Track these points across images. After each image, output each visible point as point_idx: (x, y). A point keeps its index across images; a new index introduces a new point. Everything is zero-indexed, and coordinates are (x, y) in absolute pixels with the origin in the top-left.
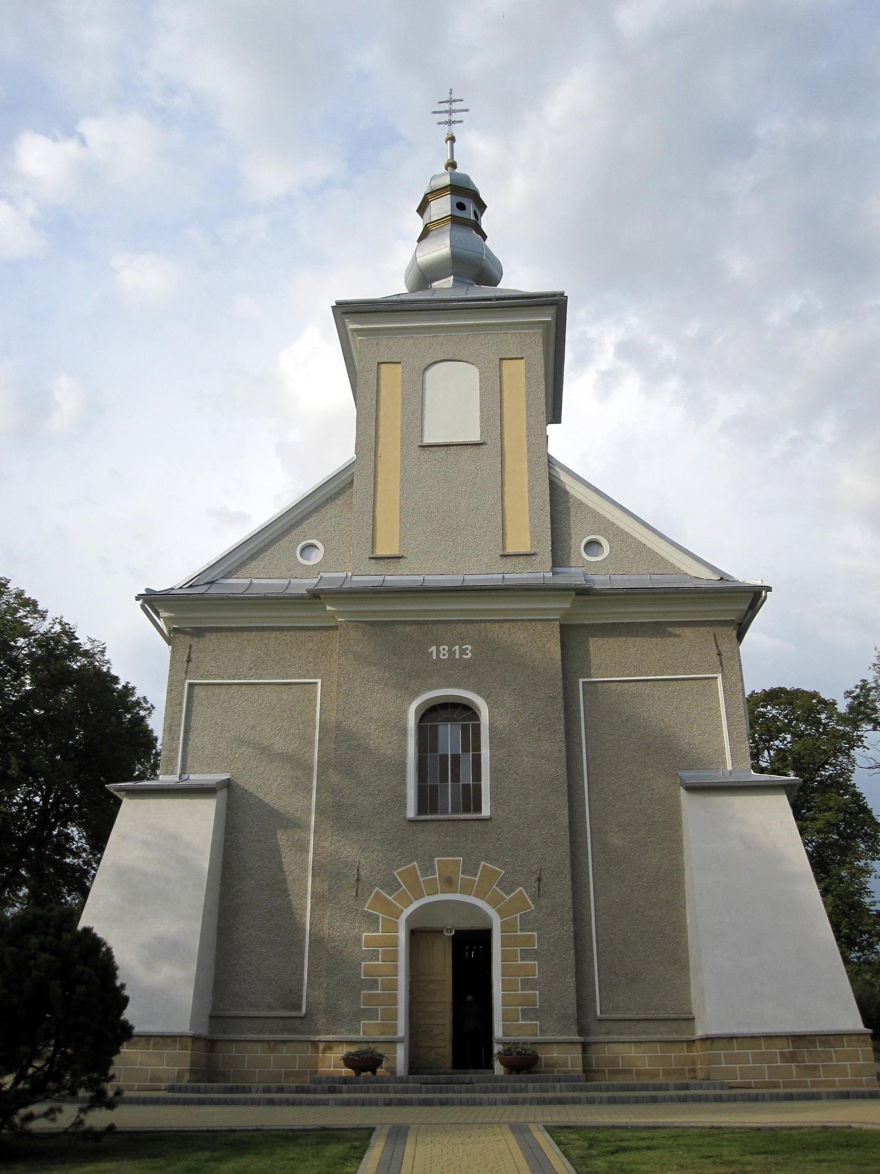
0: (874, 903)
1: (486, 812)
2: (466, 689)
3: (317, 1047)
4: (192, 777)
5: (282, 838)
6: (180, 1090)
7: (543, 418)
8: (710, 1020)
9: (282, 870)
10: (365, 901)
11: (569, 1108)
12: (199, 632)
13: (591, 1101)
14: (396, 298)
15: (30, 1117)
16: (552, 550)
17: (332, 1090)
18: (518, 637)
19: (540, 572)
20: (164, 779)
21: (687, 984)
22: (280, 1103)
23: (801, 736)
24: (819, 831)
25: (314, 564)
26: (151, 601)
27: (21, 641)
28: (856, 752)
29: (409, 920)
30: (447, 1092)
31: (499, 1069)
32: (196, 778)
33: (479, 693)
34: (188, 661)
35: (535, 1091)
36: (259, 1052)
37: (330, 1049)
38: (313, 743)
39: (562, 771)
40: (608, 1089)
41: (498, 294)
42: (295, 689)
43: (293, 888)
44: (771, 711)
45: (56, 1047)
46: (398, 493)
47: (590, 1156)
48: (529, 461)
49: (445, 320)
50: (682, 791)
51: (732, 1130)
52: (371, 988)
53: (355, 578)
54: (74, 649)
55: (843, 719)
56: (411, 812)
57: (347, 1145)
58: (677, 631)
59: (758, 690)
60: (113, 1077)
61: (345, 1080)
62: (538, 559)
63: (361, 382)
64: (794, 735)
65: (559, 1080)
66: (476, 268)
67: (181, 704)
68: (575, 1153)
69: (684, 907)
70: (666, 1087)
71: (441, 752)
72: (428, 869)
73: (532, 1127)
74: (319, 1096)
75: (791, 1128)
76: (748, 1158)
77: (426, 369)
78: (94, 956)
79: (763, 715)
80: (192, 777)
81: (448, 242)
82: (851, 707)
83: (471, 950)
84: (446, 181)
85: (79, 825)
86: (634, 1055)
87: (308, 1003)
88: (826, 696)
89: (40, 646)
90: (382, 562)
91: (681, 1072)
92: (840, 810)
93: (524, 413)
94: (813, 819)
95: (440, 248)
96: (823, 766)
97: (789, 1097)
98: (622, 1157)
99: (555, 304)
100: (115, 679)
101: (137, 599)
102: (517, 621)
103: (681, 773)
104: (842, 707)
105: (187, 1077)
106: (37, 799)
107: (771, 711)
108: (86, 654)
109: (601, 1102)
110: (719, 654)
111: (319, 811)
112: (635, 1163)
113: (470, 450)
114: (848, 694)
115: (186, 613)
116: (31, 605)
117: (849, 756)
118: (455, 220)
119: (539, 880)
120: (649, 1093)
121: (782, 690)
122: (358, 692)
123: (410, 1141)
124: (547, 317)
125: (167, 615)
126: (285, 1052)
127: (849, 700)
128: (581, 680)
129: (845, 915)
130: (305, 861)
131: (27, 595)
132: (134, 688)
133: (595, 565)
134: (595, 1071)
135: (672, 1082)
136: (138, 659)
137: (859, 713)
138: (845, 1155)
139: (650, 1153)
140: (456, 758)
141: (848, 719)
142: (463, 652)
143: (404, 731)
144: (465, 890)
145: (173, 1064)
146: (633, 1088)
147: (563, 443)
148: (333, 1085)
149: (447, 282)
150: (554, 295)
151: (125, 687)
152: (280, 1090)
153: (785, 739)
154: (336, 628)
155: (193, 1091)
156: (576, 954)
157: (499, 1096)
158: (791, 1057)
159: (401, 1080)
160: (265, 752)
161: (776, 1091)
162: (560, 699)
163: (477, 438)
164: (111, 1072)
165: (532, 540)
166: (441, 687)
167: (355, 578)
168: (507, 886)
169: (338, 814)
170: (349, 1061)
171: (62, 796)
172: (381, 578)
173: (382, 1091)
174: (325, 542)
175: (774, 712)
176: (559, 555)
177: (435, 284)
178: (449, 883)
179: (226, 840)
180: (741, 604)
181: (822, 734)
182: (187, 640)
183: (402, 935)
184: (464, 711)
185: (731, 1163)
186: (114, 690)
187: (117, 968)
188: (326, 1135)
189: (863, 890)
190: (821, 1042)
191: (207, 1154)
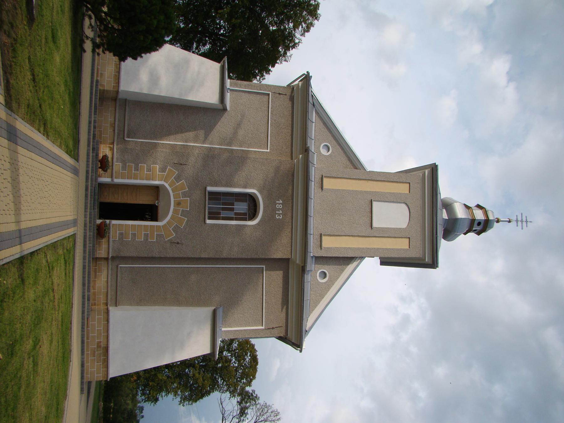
0: (162, 397)
1: (208, 221)
2: (263, 215)
3: (111, 144)
4: (229, 94)
5: (201, 133)
6: (97, 85)
7: (382, 256)
8: (116, 313)
9: (187, 131)
10: (172, 167)
11: (82, 248)
12: (292, 99)
13: (84, 258)
14: (438, 192)
15: (90, 18)
16: (323, 257)
17: (93, 149)
18: (285, 239)
19: (313, 250)
20: (228, 82)
21: (131, 305)
22: (89, 126)
23: (236, 371)
24: (194, 375)
25: (321, 151)
26: (307, 78)
27: (291, 25)
28: (228, 394)
29: (163, 185)
30: (91, 198)
31: (99, 221)
32: (228, 96)
33: (260, 221)
34: (279, 94)
35: (90, 235)
36: (110, 119)
37: (110, 150)
38: (241, 147)
39: (224, 255)
40: (89, 266)
41: (438, 238)
42: (265, 140)
43: (179, 136)
44: (248, 358)
45: (118, 30)
46: (351, 189)
47: (63, 248)
48: (363, 248)
49: (428, 214)
50: (214, 308)
51: (71, 312)
52: (135, 168)
53: (313, 168)
54: (287, 48)
55: (243, 389)
56: (209, 189)
57: (72, 149)
58: (284, 310)
59: (257, 353)
60: (104, 53)
61: (97, 155)
62: (319, 250)
63: (401, 175)
64: (237, 367)
65: (94, 246)
66: (451, 229)
67: (260, 90)
68: (65, 242)
69: (164, 305)
70: (89, 291)
71: (236, 203)
72: (184, 195)
73: (76, 228)
74: (91, 143)
75: (71, 337)
76: (60, 314)
77: (406, 204)
78: (155, 45)
79: (246, 354)
80: (229, 94)
81: (463, 217)
82: (248, 392)
83: (149, 212)
84: (491, 218)
85: (210, 49)
86: (102, 281)
87: (130, 141)
88: (254, 382)
89: (289, 33)
90: (320, 180)
91: (94, 300)
92: (203, 384)
93: (385, 247)
94: (199, 373)
95: (460, 213)
96: (223, 379)
97: (83, 342)
98: (63, 261)
99: (433, 264)
100: (273, 66)
101: (307, 72)
102: (292, 239)
103: (221, 309)
104: (248, 389)
105: (102, 88)
106: (222, 32)
107: (248, 358)
108: (285, 53)
109: (84, 262)
110: (273, 328)
111: (210, 149)
112: (60, 266)
113: (369, 222)
114: (254, 391)
115: (301, 94)
116: (308, 30)
117: (226, 391)
118: (473, 221)
119: (178, 243)
120: (87, 284)
121: (257, 363)
122: (263, 167)
123: (72, 175)
124: (427, 260)
125: (300, 85)
126: (110, 130)
127: (251, 392)
128: (264, 266)
129: (158, 384)
130: (190, 142)
131: (312, 28)
132: (269, 74)
133: (315, 275)
134: (96, 262)
135: (91, 294)
136: (281, 74)
137: (245, 396)
138: (60, 355)
139: (64, 274)
140: (232, 209)
141: (243, 391)
142: (279, 215)
143: (245, 187)
144: (175, 211)
145: (107, 84)
146: (89, 277)
147: (371, 264)
148: (95, 150)
149: (445, 216)
150: (437, 263)
151: (270, 70)
152: (95, 127)
153: (235, 363)
154: (292, 159)
155: (96, 90)
156: (145, 257)
157: (88, 219)
158: (99, 346)
159: (96, 179)
160: (239, 125)
161: (86, 338)
162: (256, 257)
163: (375, 225)
164: (107, 52)
165: (328, 248)
166: (264, 204)
167: (313, 168)
168: (176, 229)
169: (210, 156)
170: (105, 157)
171: (223, 42)
172: (313, 180)
173: (92, 170)
174: (330, 155)
175: (247, 359)
176: (320, 260)
177: (444, 211)
178: (178, 204)
179: (200, 108)
180: (294, 337)
181: (237, 380)
182: (289, 93)
183: (157, 182)
184: (253, 214)
185: (59, 306)
186: (269, 65)
187: (150, 53)
188: (77, 141)
189: (168, 392)
190: (105, 359)
191: (72, 90)
